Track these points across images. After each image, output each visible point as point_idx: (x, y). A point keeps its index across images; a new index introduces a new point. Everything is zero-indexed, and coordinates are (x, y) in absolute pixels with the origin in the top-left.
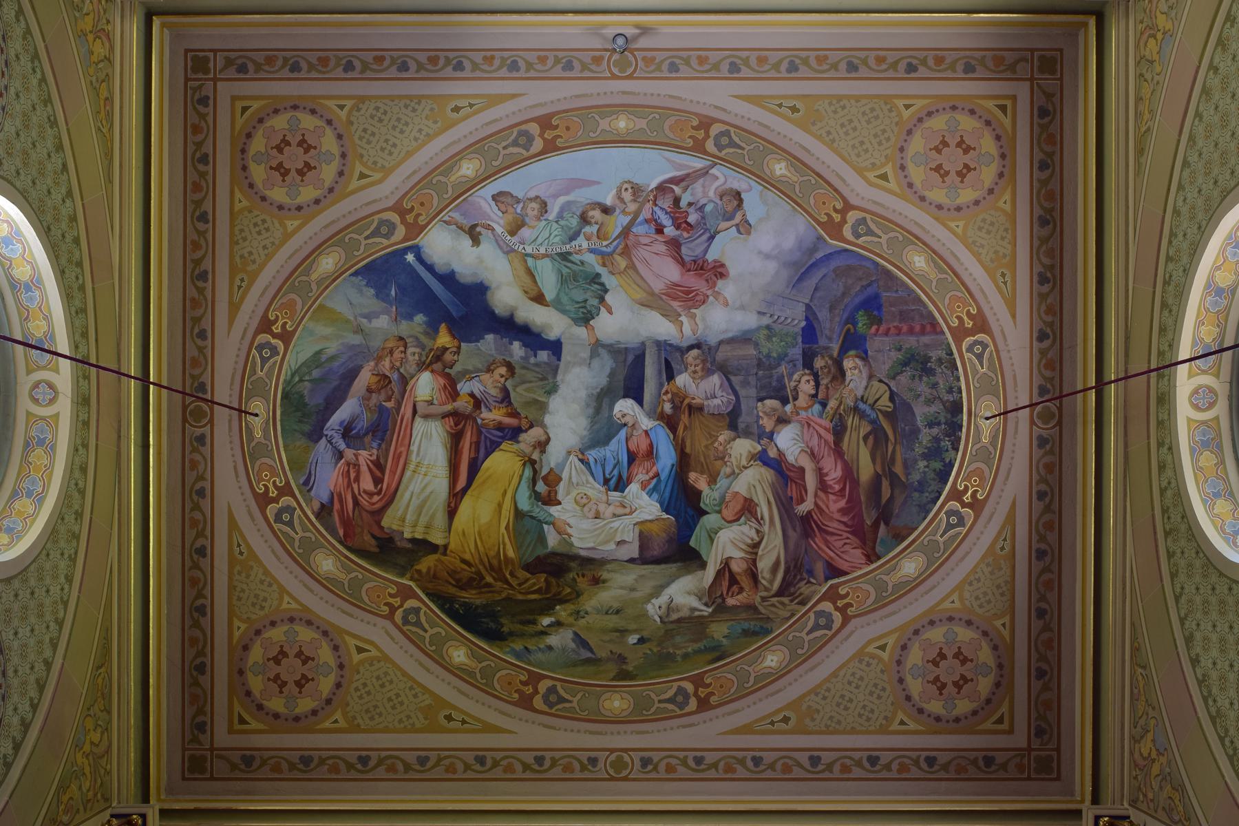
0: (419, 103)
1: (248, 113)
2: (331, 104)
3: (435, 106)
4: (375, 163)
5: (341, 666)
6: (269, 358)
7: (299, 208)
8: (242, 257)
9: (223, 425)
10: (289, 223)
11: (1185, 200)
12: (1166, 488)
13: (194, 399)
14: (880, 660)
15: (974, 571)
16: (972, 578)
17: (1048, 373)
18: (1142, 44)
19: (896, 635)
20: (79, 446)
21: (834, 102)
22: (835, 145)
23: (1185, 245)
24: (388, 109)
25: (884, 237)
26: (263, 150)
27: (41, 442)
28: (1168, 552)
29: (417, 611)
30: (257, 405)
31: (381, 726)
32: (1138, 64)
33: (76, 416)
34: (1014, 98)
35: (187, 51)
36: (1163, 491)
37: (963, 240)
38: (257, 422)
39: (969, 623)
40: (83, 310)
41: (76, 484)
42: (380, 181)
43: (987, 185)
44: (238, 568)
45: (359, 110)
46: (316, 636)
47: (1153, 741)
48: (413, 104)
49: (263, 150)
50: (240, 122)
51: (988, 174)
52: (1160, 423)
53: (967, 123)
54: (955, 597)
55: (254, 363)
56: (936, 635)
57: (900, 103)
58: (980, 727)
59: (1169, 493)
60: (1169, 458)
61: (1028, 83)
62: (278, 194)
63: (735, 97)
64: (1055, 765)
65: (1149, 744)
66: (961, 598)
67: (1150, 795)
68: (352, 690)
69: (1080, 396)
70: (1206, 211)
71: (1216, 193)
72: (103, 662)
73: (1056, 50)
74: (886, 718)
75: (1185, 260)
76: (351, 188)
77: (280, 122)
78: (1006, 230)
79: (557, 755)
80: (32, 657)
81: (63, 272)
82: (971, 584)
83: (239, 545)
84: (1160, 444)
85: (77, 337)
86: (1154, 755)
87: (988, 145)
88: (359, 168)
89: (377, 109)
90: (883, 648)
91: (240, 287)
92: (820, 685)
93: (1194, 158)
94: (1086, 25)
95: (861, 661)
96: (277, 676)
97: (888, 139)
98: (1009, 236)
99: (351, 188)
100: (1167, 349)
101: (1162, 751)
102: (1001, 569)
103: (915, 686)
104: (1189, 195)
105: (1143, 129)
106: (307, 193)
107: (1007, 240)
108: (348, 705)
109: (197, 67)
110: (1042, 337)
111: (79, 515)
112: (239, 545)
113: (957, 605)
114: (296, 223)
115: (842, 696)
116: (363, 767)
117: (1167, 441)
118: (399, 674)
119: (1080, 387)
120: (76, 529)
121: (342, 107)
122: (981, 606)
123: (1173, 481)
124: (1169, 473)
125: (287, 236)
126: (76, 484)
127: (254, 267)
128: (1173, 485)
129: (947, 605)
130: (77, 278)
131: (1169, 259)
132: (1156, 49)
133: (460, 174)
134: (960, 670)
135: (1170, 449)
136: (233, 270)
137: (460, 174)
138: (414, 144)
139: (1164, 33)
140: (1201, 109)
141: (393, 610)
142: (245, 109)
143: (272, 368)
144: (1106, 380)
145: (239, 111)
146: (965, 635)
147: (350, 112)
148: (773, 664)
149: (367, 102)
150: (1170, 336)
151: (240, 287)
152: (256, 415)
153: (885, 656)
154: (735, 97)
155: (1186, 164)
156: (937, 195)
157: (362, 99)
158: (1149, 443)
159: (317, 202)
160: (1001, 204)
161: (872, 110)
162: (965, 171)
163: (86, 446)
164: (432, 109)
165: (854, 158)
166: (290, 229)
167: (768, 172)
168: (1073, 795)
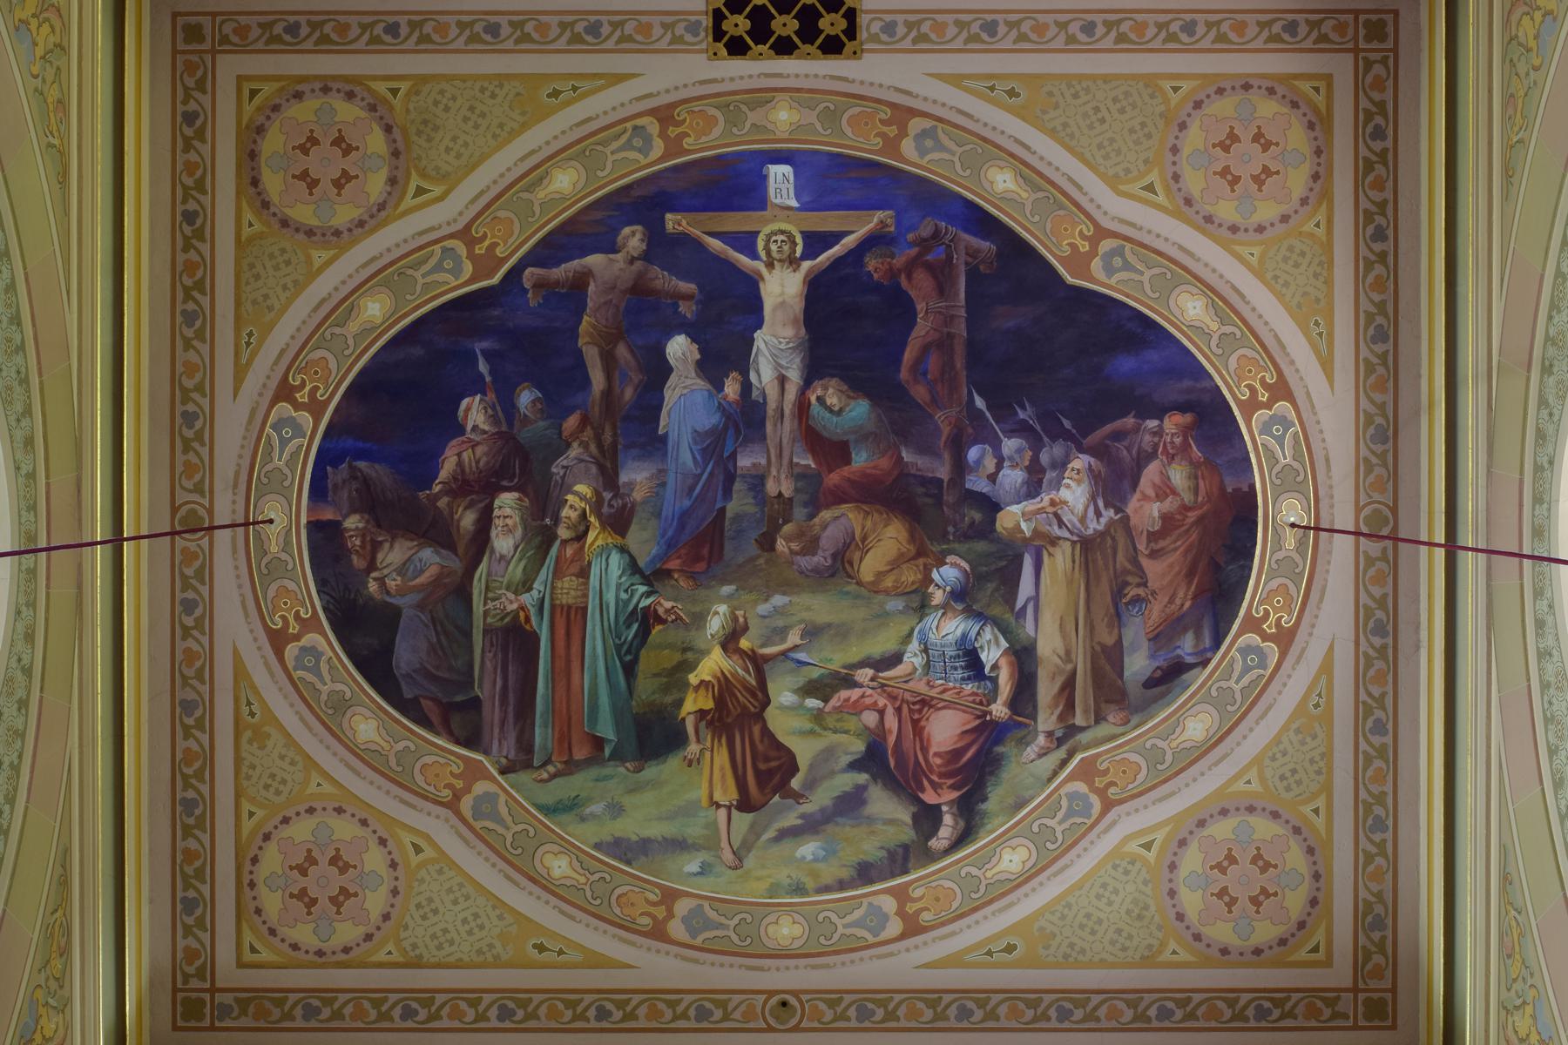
0: (501, 86)
6: (290, 439)
10: (315, 254)
12: (23, 414)
13: (1384, 533)
15: (1277, 740)
16: (1275, 750)
19: (1168, 829)
25: (1148, 274)
28: (19, 324)
30: (273, 509)
31: (452, 959)
35: (1394, 1027)
36: (28, 411)
38: (272, 530)
39: (1275, 815)
41: (1551, 415)
42: (1127, 839)
44: (248, 734)
47: (35, 44)
52: (33, 508)
54: (1253, 774)
56: (1222, 830)
57: (1167, 85)
58: (1292, 958)
59: (19, 407)
60: (19, 456)
62: (1264, 828)
63: (931, 75)
66: (1262, 780)
68: (412, 908)
69: (144, 532)
72: (1513, 148)
78: (1320, 264)
82: (1273, 759)
84: (32, 476)
85: (1549, 620)
86: (34, 23)
91: (248, 344)
96: (304, 892)
100: (24, 609)
102: (1314, 737)
105: (59, 914)
106: (344, 215)
112: (249, 704)
113: (1255, 786)
119: (145, 542)
120: (1551, 351)
121: (395, 92)
123: (14, 424)
125: (312, 275)
126: (1551, 415)
128: (13, 418)
129: (1240, 786)
130: (1550, 703)
132: (43, 1022)
135: (18, 468)
136: (1328, 719)
138: (1071, 899)
142: (253, 93)
143: (295, 455)
145: (246, 93)
149: (1137, 957)
150: (20, 627)
151: (248, 344)
152: (271, 521)
153: (1151, 856)
154: (931, 75)
156: (344, 829)
157: (424, 79)
158: (47, 477)
161: (440, 947)
164: (1047, 947)
166: (317, 263)
167: (986, 185)
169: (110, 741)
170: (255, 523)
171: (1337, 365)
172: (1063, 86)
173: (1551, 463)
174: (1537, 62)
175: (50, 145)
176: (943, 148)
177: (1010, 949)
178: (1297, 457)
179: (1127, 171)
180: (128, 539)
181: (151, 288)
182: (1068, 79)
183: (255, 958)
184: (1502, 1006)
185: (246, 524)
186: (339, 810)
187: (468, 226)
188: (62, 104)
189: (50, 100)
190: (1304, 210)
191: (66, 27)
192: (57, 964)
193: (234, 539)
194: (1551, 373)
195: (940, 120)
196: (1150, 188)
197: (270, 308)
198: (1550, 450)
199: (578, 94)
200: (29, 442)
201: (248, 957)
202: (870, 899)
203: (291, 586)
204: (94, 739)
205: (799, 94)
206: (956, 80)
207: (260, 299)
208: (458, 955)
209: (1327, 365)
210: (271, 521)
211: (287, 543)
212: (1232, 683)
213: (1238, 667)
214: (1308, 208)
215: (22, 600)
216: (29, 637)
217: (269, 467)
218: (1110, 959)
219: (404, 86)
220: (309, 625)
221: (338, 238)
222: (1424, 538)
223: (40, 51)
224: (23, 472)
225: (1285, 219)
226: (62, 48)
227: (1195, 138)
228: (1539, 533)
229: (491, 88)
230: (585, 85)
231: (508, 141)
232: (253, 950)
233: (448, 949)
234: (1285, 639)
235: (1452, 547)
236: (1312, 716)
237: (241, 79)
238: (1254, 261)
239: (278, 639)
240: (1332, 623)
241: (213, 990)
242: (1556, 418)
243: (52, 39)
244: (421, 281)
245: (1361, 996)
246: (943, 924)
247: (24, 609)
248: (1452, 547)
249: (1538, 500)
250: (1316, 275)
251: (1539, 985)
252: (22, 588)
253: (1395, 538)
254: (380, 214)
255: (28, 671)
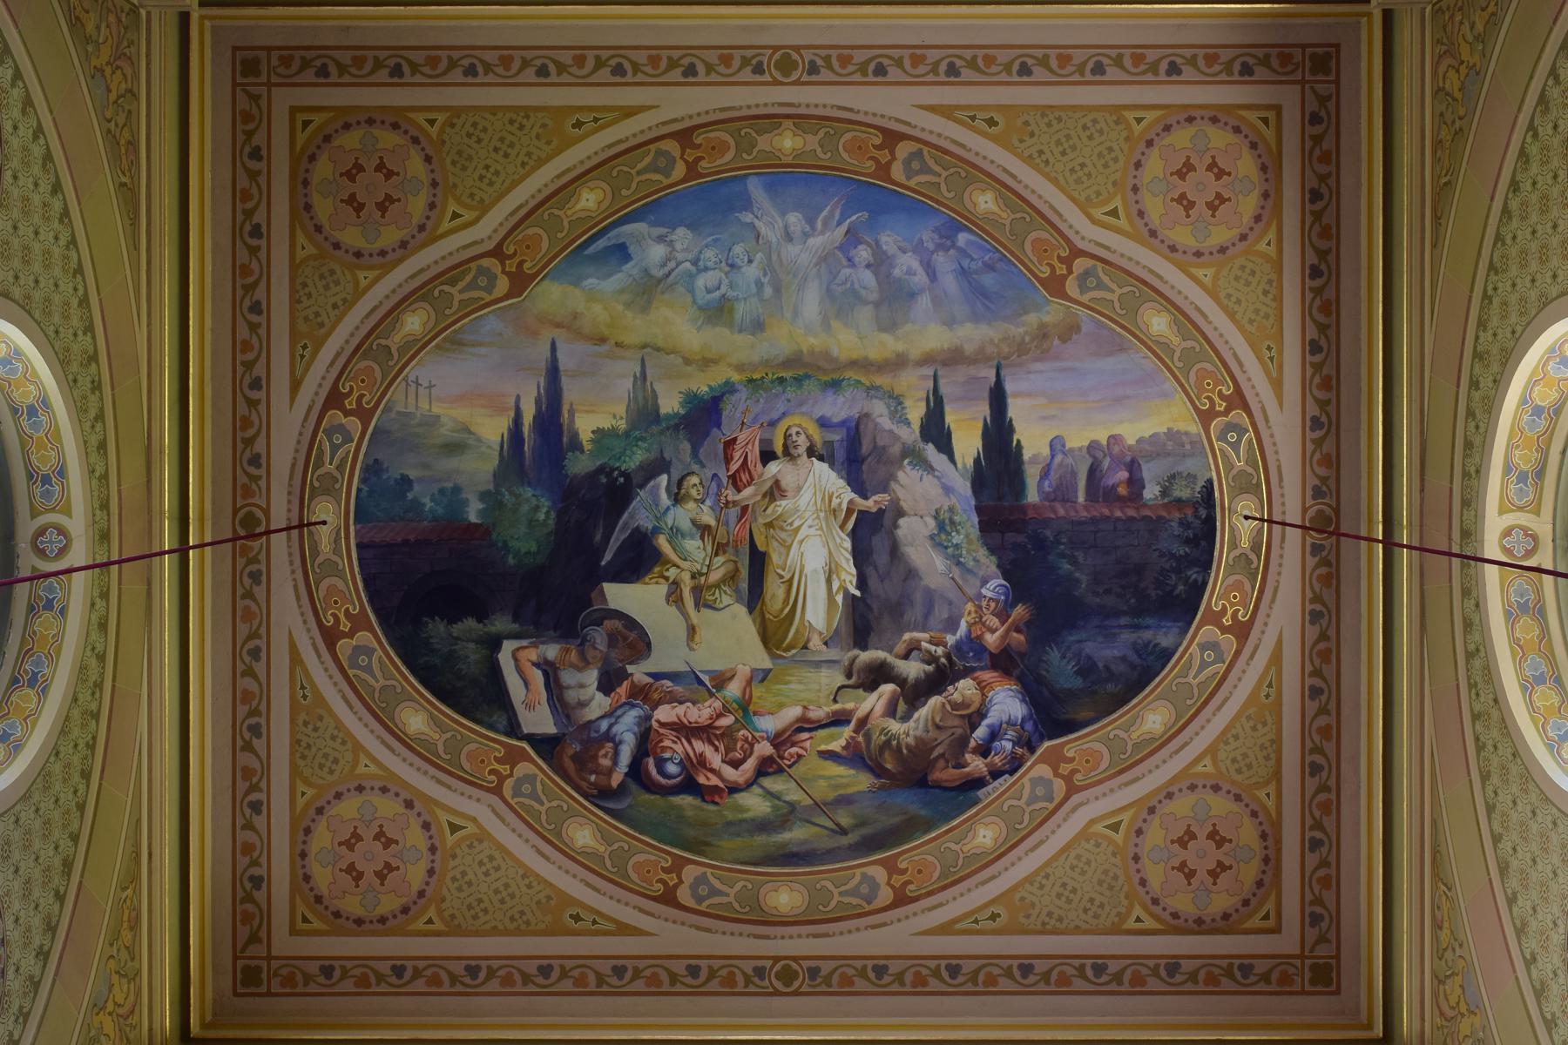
1: (311, 128)
2: (420, 118)
3: (1023, 920)
4: (1098, 845)
5: (433, 849)
6: (341, 446)
7: (1193, 787)
8: (1265, 724)
9: (1292, 505)
10: (1210, 769)
11: (75, 792)
12: (96, 419)
13: (1328, 529)
14: (458, 200)
17: (1322, 471)
18: (132, 998)
20: (1475, 475)
21: (523, 927)
22: (521, 872)
23: (76, 732)
24: (1083, 916)
26: (331, 178)
27: (1522, 478)
29: (531, 779)
30: (325, 510)
32: (138, 972)
33: (1479, 517)
34: (1278, 109)
36: (100, 417)
37: (1213, 294)
40: (1470, 656)
41: (1477, 427)
42: (1093, 822)
43: (323, 822)
44: (303, 716)
45: (1118, 914)
46: (1167, 232)
47: (109, 91)
48: (1053, 922)
49: (331, 178)
50: (301, 138)
51: (1248, 204)
52: (105, 506)
53: (1219, 138)
55: (321, 451)
57: (1130, 116)
59: (92, 414)
61: (1298, 87)
63: (921, 107)
64: (238, 68)
65: (113, 86)
67: (112, 19)
69: (208, 539)
70: (49, 774)
71: (36, 797)
72: (1443, 191)
73: (1331, 45)
74: (453, 126)
75: (76, 713)
76: (1131, 812)
77: (350, 140)
79: (717, 963)
80: (1534, 198)
81: (1496, 701)
83: (303, 687)
84: (105, 477)
86: (108, 71)
87: (1246, 166)
88: (1119, 837)
89: (1096, 916)
90: (455, 216)
92: (1036, 873)
93: (66, 843)
94: (204, 1026)
95: (482, 201)
97: (1116, 160)
98: (1273, 291)
99: (1131, 812)
101: (98, 74)
103: (416, 166)
104: (71, 797)
106: (390, 236)
107: (1270, 296)
108: (443, 900)
109: (1324, 975)
110: (1316, 423)
111: (1474, 384)
114: (1199, 768)
115: (506, 156)
116: (473, 976)
117: (95, 482)
118: (1062, 182)
119: (208, 549)
121: (432, 122)
122: (332, 272)
124: (94, 440)
127: (1251, 711)
131: (96, 716)
132: (116, 990)
133: (578, 207)
134: (1219, 855)
137: (578, 207)
138: (521, 171)
139: (104, 1008)
140: (56, 907)
141: (502, 779)
142: (306, 124)
144: (175, 556)
145: (299, 125)
146: (1220, 805)
147: (1129, 913)
148: (591, 205)
152: (324, 523)
154: (921, 107)
155: (75, 838)
156: (388, 807)
157: (457, 111)
159: (1170, 796)
160: (310, 792)
161: (475, 917)
162: (1217, 202)
163: (1466, 474)
164: (1028, 917)
165: (497, 854)
166: (1207, 761)
168: (214, 29)
169: (176, 524)
170: (310, 524)
171: (1286, 387)
172: (1038, 117)
173: (1478, 472)
174: (1462, 112)
175: (123, 185)
176: (929, 171)
177: (994, 917)
178: (1251, 461)
179: (1098, 193)
180: (194, 547)
181: (213, 704)
182: (1044, 110)
183: (306, 926)
184: (1435, 975)
185: (301, 526)
186: (384, 790)
187: (500, 245)
188: (133, 145)
189: (123, 142)
190: (1259, 227)
191: (136, 76)
192: (127, 936)
193: (289, 539)
194: (1477, 389)
195: (926, 143)
196: (1114, 213)
197: (322, 325)
198: (1477, 459)
199: (599, 124)
200: (102, 446)
201: (300, 925)
202: (864, 870)
203: (340, 584)
204: (162, 452)
205: (802, 120)
206: (946, 111)
207: (312, 316)
208: (493, 923)
209: (1277, 384)
210: (324, 523)
211: (337, 541)
212: (1190, 679)
213: (1196, 663)
214: (1261, 225)
215: (96, 593)
216: (103, 626)
217: (320, 472)
218: (1084, 926)
219: (441, 118)
220: (359, 623)
221: (386, 259)
222: (1364, 533)
223: (113, 96)
224: (97, 474)
225: (1243, 237)
226: (132, 94)
227: (1154, 166)
228: (1466, 534)
229: (519, 119)
230: (611, 116)
231: (534, 169)
232: (305, 920)
233: (483, 918)
234: (1242, 631)
235: (1390, 544)
236: (1265, 706)
237: (294, 110)
238: (1207, 281)
239: (331, 637)
240: (1283, 619)
241: (269, 958)
242: (1482, 430)
243: (123, 86)
244: (458, 297)
245: (1308, 962)
246: (930, 894)
247: (98, 600)
248: (1390, 544)
249: (1466, 503)
250: (1265, 293)
251: (1467, 957)
252: (96, 494)
253: (1337, 533)
254: (425, 233)
255: (101, 658)
